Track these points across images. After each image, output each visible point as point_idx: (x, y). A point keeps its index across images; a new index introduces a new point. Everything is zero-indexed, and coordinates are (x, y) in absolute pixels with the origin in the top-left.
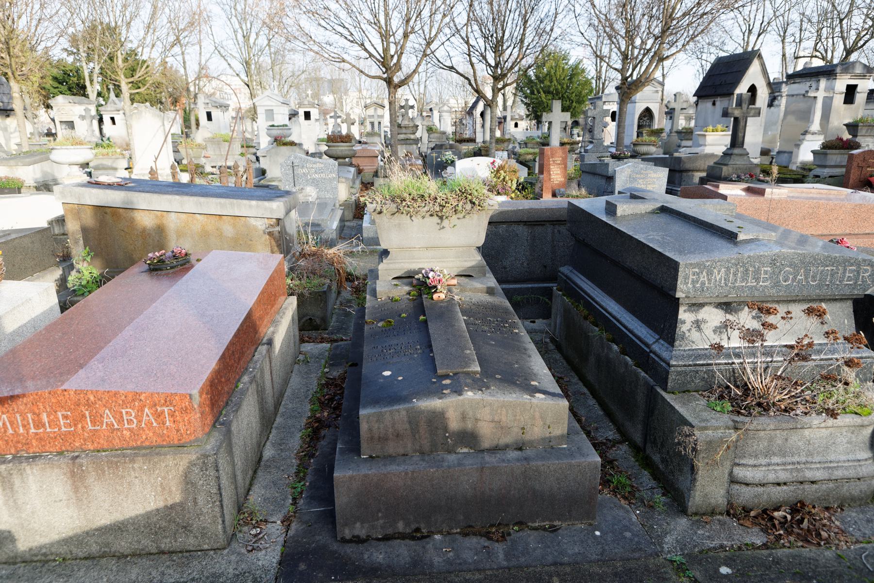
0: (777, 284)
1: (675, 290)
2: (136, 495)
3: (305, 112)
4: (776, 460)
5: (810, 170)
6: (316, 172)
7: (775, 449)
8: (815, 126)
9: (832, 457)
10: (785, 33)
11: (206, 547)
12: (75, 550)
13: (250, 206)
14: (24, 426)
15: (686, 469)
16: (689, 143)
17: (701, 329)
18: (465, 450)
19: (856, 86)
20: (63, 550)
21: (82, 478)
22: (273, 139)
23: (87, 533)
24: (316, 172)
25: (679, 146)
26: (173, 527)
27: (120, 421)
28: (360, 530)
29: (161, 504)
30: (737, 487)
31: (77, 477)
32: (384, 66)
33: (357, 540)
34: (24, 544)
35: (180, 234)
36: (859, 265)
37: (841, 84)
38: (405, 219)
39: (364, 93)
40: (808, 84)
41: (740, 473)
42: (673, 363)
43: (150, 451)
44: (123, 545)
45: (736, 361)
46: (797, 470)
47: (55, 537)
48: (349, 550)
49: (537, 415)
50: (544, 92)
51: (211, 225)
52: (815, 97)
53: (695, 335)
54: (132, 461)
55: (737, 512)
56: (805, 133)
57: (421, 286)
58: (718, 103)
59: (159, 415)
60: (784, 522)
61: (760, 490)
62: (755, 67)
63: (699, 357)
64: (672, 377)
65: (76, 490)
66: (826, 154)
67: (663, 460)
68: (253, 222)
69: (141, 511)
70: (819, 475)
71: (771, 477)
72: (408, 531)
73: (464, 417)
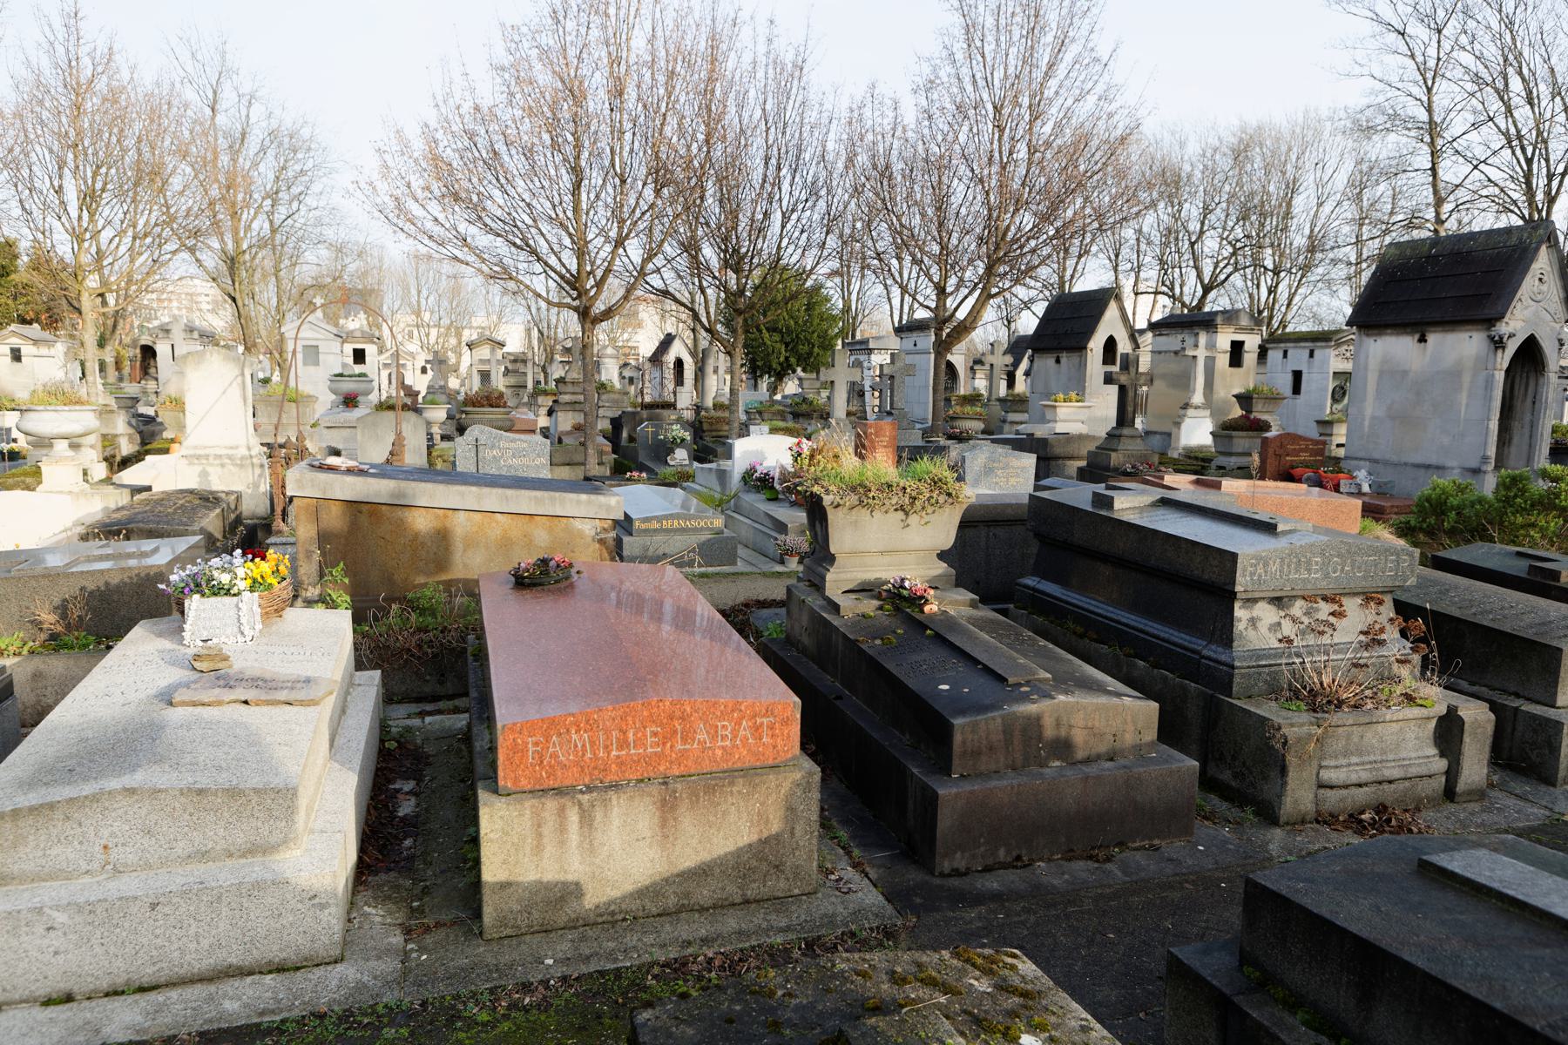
0: (1327, 576)
1: (1234, 583)
2: (724, 831)
3: (355, 351)
4: (1354, 759)
5: (1209, 460)
6: (514, 456)
7: (1352, 747)
8: (1198, 398)
9: (1403, 754)
10: (1117, 256)
11: (796, 891)
12: (648, 905)
13: (579, 502)
14: (606, 747)
15: (1274, 774)
16: (1024, 417)
17: (1257, 628)
18: (1057, 763)
19: (1242, 343)
20: (635, 905)
21: (673, 808)
22: (341, 399)
23: (667, 880)
24: (514, 456)
25: (1004, 421)
26: (764, 867)
27: (714, 737)
28: (959, 861)
29: (755, 838)
30: (1322, 791)
31: (667, 807)
32: (575, 289)
33: (956, 873)
34: (594, 898)
35: (470, 543)
36: (1398, 555)
37: (1224, 339)
38: (865, 513)
39: (426, 317)
40: (1180, 337)
41: (1327, 775)
42: (1237, 664)
43: (750, 773)
44: (704, 895)
45: (1297, 661)
46: (1377, 770)
47: (629, 887)
48: (955, 882)
49: (1129, 719)
50: (768, 330)
51: (516, 528)
52: (1195, 357)
53: (1251, 634)
54: (732, 784)
55: (1326, 819)
56: (1186, 406)
57: (901, 601)
58: (1064, 360)
59: (757, 729)
60: (1373, 823)
61: (1344, 792)
62: (1112, 311)
63: (1259, 658)
64: (1237, 680)
65: (664, 823)
66: (1231, 437)
67: (1235, 776)
68: (577, 524)
69: (730, 846)
70: (1396, 773)
71: (1354, 778)
72: (1009, 859)
73: (1058, 725)
